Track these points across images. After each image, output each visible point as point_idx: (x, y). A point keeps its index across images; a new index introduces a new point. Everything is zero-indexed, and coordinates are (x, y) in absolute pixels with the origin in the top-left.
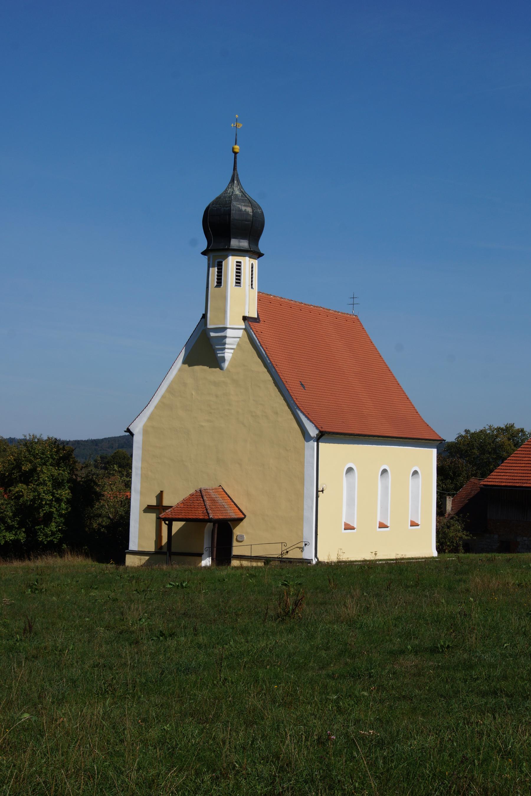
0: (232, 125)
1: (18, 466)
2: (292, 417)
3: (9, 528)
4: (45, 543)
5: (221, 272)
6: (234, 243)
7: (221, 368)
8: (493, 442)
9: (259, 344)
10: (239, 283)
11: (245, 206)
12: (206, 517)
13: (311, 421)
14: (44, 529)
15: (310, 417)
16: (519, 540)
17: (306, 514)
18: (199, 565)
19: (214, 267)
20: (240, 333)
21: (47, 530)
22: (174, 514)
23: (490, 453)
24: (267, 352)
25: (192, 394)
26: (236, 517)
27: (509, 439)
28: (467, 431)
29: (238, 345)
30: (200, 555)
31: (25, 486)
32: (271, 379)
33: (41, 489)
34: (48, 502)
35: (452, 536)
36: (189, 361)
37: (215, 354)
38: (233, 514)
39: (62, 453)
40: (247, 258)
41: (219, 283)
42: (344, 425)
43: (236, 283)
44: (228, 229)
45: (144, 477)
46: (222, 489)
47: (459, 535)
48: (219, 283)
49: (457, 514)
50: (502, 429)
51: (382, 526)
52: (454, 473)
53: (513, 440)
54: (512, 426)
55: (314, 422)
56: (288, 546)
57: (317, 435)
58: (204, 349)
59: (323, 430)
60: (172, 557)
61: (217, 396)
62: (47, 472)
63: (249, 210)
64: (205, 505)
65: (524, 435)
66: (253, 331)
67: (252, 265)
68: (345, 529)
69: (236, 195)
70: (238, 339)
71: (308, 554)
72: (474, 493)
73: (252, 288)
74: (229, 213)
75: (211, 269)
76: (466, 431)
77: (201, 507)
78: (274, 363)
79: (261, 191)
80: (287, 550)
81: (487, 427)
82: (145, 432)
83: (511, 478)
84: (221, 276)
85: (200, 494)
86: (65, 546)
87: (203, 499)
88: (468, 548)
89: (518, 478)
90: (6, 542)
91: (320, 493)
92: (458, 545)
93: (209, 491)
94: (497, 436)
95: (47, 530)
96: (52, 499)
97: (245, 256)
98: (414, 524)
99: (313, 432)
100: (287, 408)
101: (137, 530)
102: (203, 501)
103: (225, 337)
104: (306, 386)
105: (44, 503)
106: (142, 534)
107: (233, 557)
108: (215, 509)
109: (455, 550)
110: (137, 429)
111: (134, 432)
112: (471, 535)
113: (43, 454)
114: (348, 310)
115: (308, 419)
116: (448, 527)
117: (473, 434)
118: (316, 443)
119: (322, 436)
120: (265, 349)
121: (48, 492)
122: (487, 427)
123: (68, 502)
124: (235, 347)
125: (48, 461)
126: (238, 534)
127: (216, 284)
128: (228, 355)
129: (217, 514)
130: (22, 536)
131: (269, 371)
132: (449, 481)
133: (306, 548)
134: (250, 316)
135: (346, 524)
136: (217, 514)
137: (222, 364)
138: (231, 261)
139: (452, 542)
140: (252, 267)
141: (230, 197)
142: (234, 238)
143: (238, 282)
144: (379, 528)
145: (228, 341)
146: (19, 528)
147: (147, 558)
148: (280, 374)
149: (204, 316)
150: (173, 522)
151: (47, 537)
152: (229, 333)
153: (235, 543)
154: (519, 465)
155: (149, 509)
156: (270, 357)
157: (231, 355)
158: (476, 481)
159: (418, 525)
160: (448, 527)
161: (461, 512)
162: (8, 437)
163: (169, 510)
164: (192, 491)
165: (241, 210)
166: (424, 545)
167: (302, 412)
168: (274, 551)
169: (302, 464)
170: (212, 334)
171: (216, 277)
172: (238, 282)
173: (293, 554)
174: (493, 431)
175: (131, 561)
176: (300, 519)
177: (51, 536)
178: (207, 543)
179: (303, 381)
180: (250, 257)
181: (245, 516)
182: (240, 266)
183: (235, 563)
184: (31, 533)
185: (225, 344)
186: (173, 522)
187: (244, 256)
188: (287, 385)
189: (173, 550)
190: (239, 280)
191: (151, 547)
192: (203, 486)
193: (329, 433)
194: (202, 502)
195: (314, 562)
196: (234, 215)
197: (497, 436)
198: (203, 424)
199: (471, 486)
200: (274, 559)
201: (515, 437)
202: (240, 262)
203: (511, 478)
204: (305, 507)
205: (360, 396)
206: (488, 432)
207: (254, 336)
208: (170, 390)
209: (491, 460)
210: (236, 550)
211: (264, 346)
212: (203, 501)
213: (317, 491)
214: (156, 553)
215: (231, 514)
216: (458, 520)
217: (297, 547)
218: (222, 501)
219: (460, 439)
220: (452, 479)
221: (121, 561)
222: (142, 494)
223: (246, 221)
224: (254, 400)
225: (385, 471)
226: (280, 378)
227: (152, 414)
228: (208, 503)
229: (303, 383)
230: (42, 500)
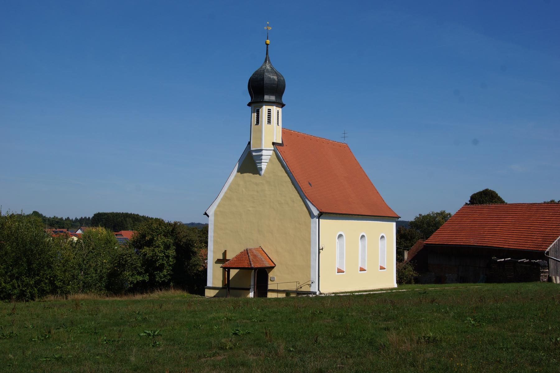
1: (144, 236)
2: (303, 203)
3: (139, 274)
6: (267, 98)
7: (260, 175)
12: (250, 266)
16: (447, 275)
17: (312, 263)
18: (248, 296)
19: (254, 112)
20: (271, 153)
21: (161, 274)
23: (432, 226)
28: (420, 215)
29: (270, 160)
30: (248, 289)
31: (148, 248)
33: (156, 250)
36: (241, 170)
37: (256, 166)
38: (267, 264)
39: (173, 230)
40: (275, 107)
41: (258, 122)
44: (263, 90)
45: (215, 242)
47: (411, 273)
48: (258, 122)
49: (410, 261)
51: (362, 270)
52: (411, 237)
54: (444, 212)
56: (301, 283)
58: (249, 163)
60: (231, 291)
61: (257, 192)
62: (160, 240)
63: (275, 78)
71: (314, 288)
74: (263, 79)
79: (282, 66)
82: (216, 214)
86: (172, 284)
88: (417, 281)
90: (137, 281)
92: (411, 279)
94: (436, 217)
95: (161, 274)
99: (316, 212)
103: (262, 155)
106: (214, 277)
109: (409, 282)
110: (211, 212)
114: (342, 141)
115: (313, 204)
119: (321, 215)
123: (174, 257)
124: (268, 161)
125: (161, 233)
128: (264, 166)
130: (147, 278)
131: (288, 175)
132: (408, 242)
135: (381, 267)
141: (264, 70)
142: (267, 95)
143: (269, 122)
145: (263, 157)
146: (145, 273)
147: (217, 291)
149: (249, 143)
151: (161, 278)
152: (264, 153)
153: (269, 282)
155: (218, 261)
158: (422, 242)
160: (405, 269)
161: (414, 260)
164: (242, 250)
165: (270, 78)
166: (388, 280)
167: (309, 200)
169: (310, 233)
170: (254, 154)
172: (269, 122)
173: (304, 289)
175: (209, 293)
176: (309, 267)
178: (252, 283)
183: (270, 295)
184: (152, 276)
185: (262, 159)
189: (230, 286)
191: (220, 285)
192: (249, 247)
193: (326, 213)
195: (318, 294)
196: (266, 81)
197: (436, 217)
199: (419, 244)
200: (293, 292)
204: (312, 259)
208: (230, 189)
210: (270, 287)
213: (319, 249)
220: (410, 240)
221: (203, 294)
222: (214, 252)
225: (363, 236)
227: (219, 203)
228: (251, 258)
230: (157, 256)
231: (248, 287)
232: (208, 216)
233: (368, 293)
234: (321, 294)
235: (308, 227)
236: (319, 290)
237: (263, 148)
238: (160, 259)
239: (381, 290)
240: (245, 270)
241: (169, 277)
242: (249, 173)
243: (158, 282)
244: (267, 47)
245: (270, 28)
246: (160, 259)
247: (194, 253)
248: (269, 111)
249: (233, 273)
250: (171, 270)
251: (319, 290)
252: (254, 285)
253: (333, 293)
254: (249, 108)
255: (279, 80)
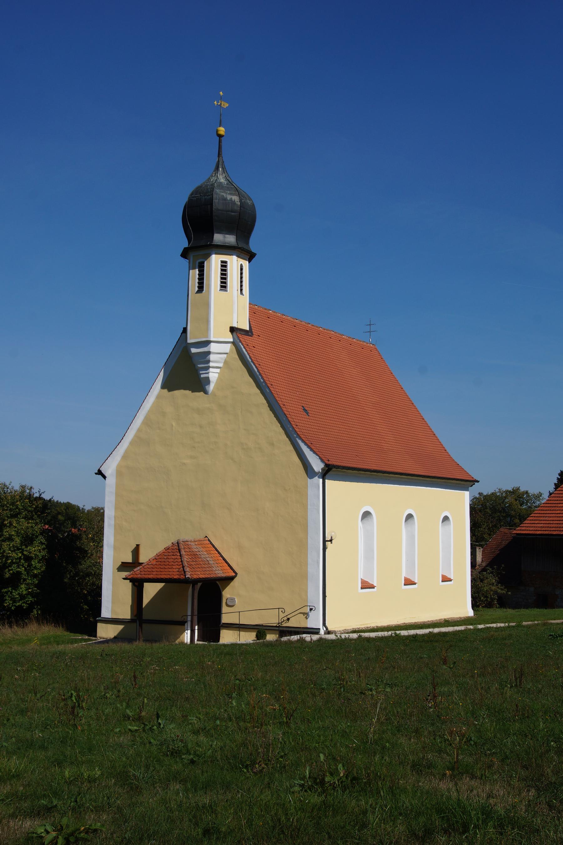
0: (215, 103)
2: (292, 448)
4: (13, 608)
5: (203, 275)
6: (218, 238)
7: (206, 392)
8: (503, 502)
9: (250, 360)
10: (225, 287)
11: (231, 194)
12: (183, 577)
13: (315, 452)
14: (11, 593)
15: (313, 447)
17: (311, 570)
19: (194, 268)
20: (228, 348)
21: (15, 594)
22: (143, 573)
23: (500, 512)
24: (260, 369)
25: (172, 426)
26: (223, 575)
27: (516, 500)
28: (480, 494)
29: (226, 362)
30: (182, 623)
32: (265, 401)
34: (14, 561)
35: (487, 591)
38: (220, 572)
40: (235, 257)
41: (201, 288)
42: (358, 458)
43: (222, 287)
44: (210, 225)
45: (118, 529)
46: (209, 540)
47: (493, 588)
48: (201, 288)
50: (510, 492)
53: (519, 501)
54: (518, 489)
55: (318, 453)
56: (288, 611)
57: (322, 469)
58: (185, 370)
59: (330, 463)
60: (144, 625)
61: (201, 427)
63: (236, 198)
64: (182, 561)
65: (528, 496)
66: (242, 344)
67: (241, 266)
68: (362, 588)
69: (221, 183)
70: (225, 355)
71: (315, 621)
72: (504, 543)
73: (241, 293)
74: (210, 202)
75: (191, 271)
76: (479, 493)
77: (177, 563)
78: (268, 382)
80: (288, 617)
81: (497, 490)
82: (119, 473)
83: (547, 525)
84: (203, 279)
85: (177, 547)
87: (180, 553)
89: (554, 525)
91: (328, 544)
93: (189, 543)
94: (505, 498)
95: (15, 594)
96: (20, 557)
97: (232, 255)
98: (445, 579)
99: (317, 466)
100: (285, 437)
101: (110, 593)
102: (181, 556)
103: (209, 353)
104: (310, 412)
105: (9, 561)
106: (115, 599)
107: (222, 626)
108: (194, 566)
110: (110, 469)
111: (106, 475)
112: (506, 590)
113: (13, 504)
115: (312, 450)
116: (482, 581)
117: (485, 496)
118: (321, 480)
119: (329, 471)
120: (257, 365)
121: (16, 549)
122: (497, 490)
124: (221, 365)
125: (20, 513)
126: (229, 596)
127: (197, 289)
128: (213, 375)
129: (197, 573)
133: (311, 614)
134: (240, 327)
135: (363, 582)
136: (197, 573)
137: (207, 387)
138: (215, 260)
139: (486, 597)
140: (241, 269)
141: (213, 185)
143: (224, 286)
144: (405, 585)
145: (212, 357)
147: (121, 627)
148: (276, 395)
149: (185, 330)
150: (145, 584)
152: (213, 347)
153: (225, 609)
154: (554, 512)
155: (124, 567)
156: (264, 375)
157: (217, 375)
158: (506, 531)
159: (450, 580)
160: (482, 581)
162: (65, 502)
163: (138, 568)
164: (169, 544)
165: (225, 199)
167: (303, 441)
168: (271, 619)
170: (194, 350)
171: (197, 281)
172: (224, 286)
174: (502, 494)
175: (106, 632)
176: (304, 576)
177: (21, 600)
179: (306, 406)
180: (238, 256)
181: (236, 574)
182: (226, 266)
183: (227, 637)
185: (209, 361)
186: (145, 584)
187: (230, 255)
188: (284, 409)
190: (225, 283)
191: (126, 614)
192: (185, 536)
193: (338, 467)
194: (179, 557)
196: (217, 204)
197: (505, 498)
198: (185, 461)
199: (502, 536)
201: (520, 498)
202: (226, 262)
203: (547, 525)
205: (379, 428)
206: (498, 494)
207: (244, 350)
208: (147, 422)
209: (501, 518)
210: (225, 619)
211: (256, 362)
212: (181, 556)
213: (324, 541)
214: (132, 621)
215: (217, 572)
216: (492, 573)
217: (300, 613)
218: (207, 556)
219: (475, 500)
221: (93, 632)
222: (115, 548)
223: (232, 212)
224: (245, 430)
225: (410, 517)
226: (276, 400)
227: (126, 452)
228: (186, 558)
229: (306, 409)
230: (7, 558)
231: (179, 618)
232: (104, 477)
233: (427, 631)
234: (328, 632)
235: (303, 494)
236: (324, 624)
237: (212, 339)
238: (12, 563)
239: (447, 623)
240: (175, 584)
241: (30, 599)
242: (185, 389)
243: (9, 609)
244: (220, 142)
245: (225, 105)
246: (12, 563)
247: (84, 553)
248: (224, 265)
249: (151, 590)
250: (36, 586)
251: (324, 624)
252: (192, 616)
253: (354, 632)
254: (185, 262)
255: (243, 205)
